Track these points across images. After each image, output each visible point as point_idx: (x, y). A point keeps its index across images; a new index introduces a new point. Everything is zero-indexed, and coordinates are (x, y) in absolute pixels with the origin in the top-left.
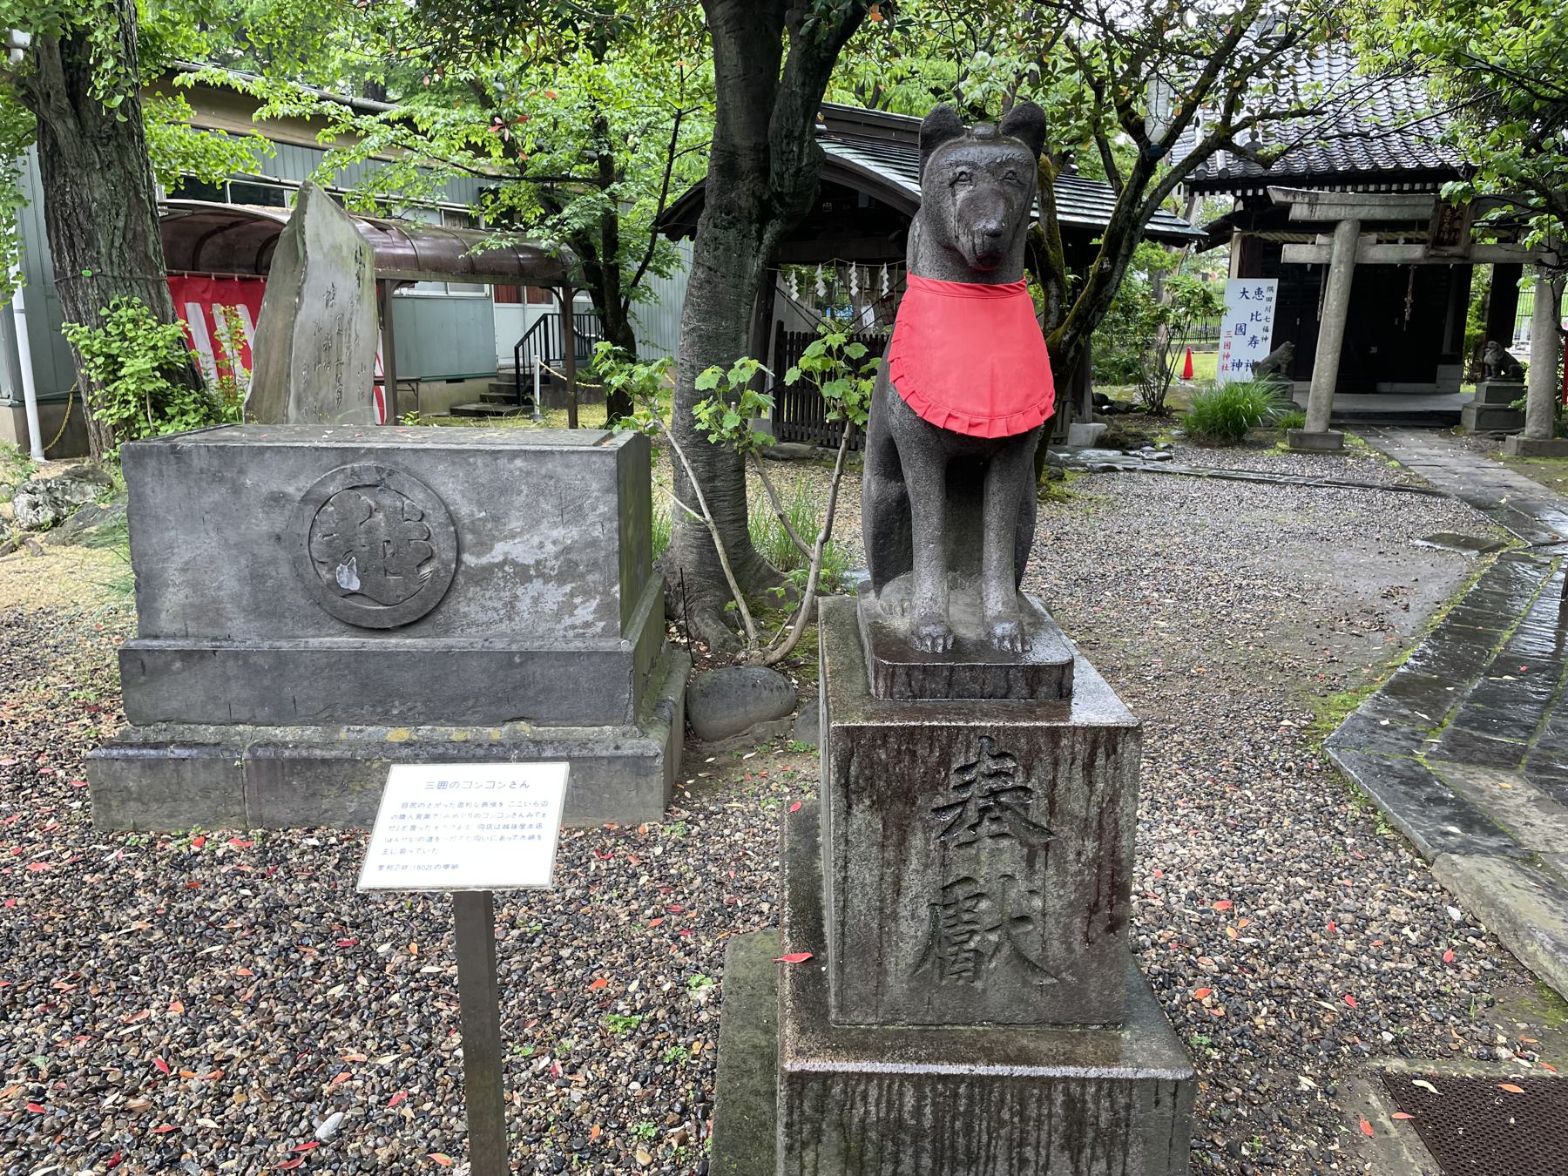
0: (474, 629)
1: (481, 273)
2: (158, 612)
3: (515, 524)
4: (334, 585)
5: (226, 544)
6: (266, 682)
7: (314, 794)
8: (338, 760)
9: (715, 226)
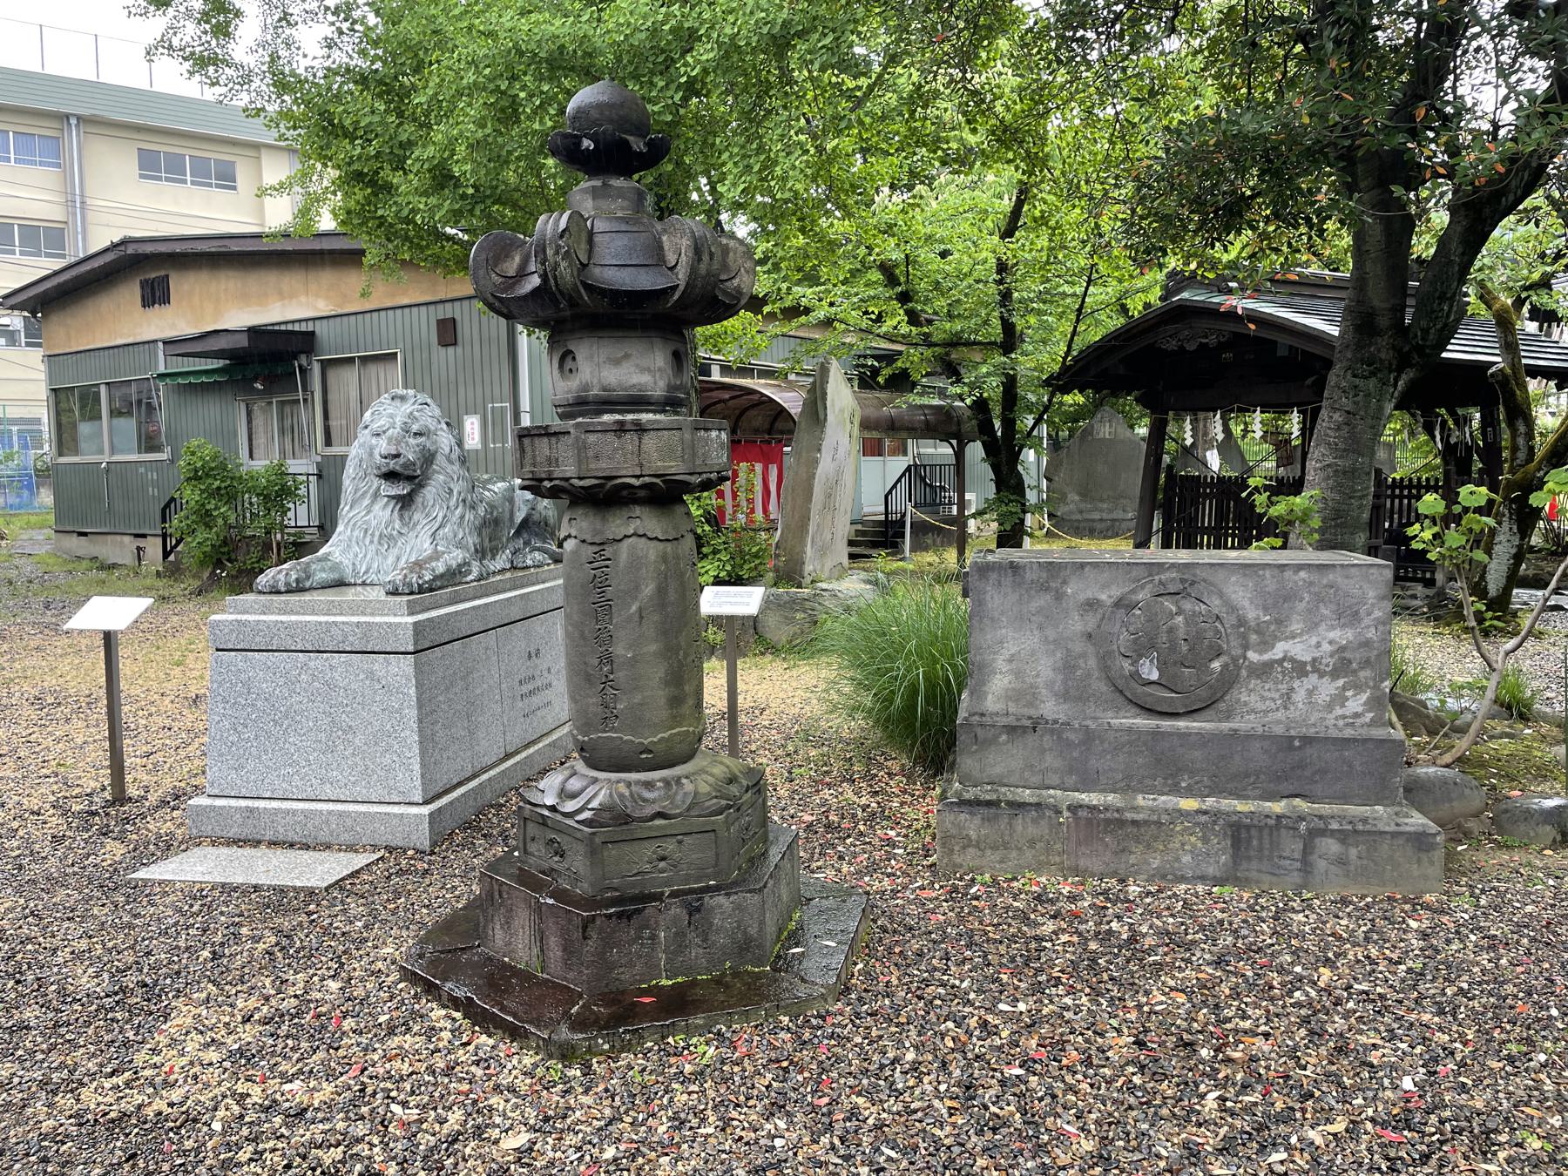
0: (1252, 717)
1: (900, 429)
2: (986, 693)
3: (1296, 626)
4: (1135, 676)
5: (1046, 641)
6: (1075, 754)
7: (1123, 851)
8: (1146, 822)
9: (1355, 376)
